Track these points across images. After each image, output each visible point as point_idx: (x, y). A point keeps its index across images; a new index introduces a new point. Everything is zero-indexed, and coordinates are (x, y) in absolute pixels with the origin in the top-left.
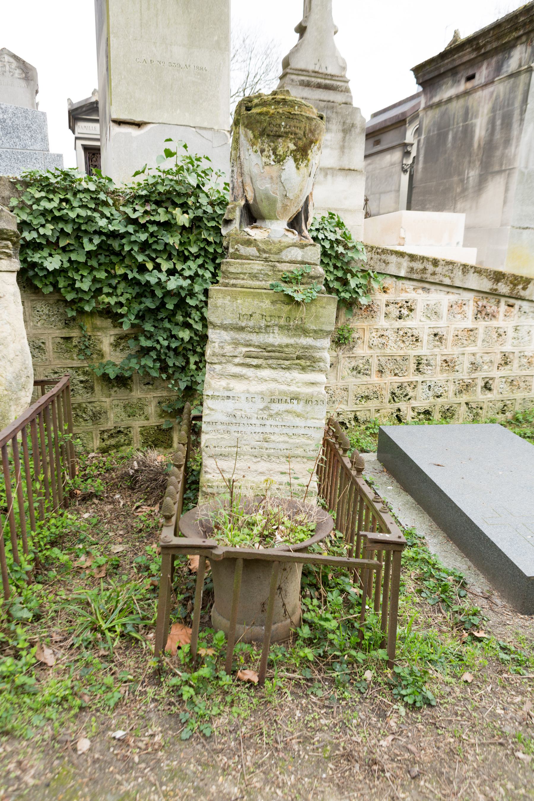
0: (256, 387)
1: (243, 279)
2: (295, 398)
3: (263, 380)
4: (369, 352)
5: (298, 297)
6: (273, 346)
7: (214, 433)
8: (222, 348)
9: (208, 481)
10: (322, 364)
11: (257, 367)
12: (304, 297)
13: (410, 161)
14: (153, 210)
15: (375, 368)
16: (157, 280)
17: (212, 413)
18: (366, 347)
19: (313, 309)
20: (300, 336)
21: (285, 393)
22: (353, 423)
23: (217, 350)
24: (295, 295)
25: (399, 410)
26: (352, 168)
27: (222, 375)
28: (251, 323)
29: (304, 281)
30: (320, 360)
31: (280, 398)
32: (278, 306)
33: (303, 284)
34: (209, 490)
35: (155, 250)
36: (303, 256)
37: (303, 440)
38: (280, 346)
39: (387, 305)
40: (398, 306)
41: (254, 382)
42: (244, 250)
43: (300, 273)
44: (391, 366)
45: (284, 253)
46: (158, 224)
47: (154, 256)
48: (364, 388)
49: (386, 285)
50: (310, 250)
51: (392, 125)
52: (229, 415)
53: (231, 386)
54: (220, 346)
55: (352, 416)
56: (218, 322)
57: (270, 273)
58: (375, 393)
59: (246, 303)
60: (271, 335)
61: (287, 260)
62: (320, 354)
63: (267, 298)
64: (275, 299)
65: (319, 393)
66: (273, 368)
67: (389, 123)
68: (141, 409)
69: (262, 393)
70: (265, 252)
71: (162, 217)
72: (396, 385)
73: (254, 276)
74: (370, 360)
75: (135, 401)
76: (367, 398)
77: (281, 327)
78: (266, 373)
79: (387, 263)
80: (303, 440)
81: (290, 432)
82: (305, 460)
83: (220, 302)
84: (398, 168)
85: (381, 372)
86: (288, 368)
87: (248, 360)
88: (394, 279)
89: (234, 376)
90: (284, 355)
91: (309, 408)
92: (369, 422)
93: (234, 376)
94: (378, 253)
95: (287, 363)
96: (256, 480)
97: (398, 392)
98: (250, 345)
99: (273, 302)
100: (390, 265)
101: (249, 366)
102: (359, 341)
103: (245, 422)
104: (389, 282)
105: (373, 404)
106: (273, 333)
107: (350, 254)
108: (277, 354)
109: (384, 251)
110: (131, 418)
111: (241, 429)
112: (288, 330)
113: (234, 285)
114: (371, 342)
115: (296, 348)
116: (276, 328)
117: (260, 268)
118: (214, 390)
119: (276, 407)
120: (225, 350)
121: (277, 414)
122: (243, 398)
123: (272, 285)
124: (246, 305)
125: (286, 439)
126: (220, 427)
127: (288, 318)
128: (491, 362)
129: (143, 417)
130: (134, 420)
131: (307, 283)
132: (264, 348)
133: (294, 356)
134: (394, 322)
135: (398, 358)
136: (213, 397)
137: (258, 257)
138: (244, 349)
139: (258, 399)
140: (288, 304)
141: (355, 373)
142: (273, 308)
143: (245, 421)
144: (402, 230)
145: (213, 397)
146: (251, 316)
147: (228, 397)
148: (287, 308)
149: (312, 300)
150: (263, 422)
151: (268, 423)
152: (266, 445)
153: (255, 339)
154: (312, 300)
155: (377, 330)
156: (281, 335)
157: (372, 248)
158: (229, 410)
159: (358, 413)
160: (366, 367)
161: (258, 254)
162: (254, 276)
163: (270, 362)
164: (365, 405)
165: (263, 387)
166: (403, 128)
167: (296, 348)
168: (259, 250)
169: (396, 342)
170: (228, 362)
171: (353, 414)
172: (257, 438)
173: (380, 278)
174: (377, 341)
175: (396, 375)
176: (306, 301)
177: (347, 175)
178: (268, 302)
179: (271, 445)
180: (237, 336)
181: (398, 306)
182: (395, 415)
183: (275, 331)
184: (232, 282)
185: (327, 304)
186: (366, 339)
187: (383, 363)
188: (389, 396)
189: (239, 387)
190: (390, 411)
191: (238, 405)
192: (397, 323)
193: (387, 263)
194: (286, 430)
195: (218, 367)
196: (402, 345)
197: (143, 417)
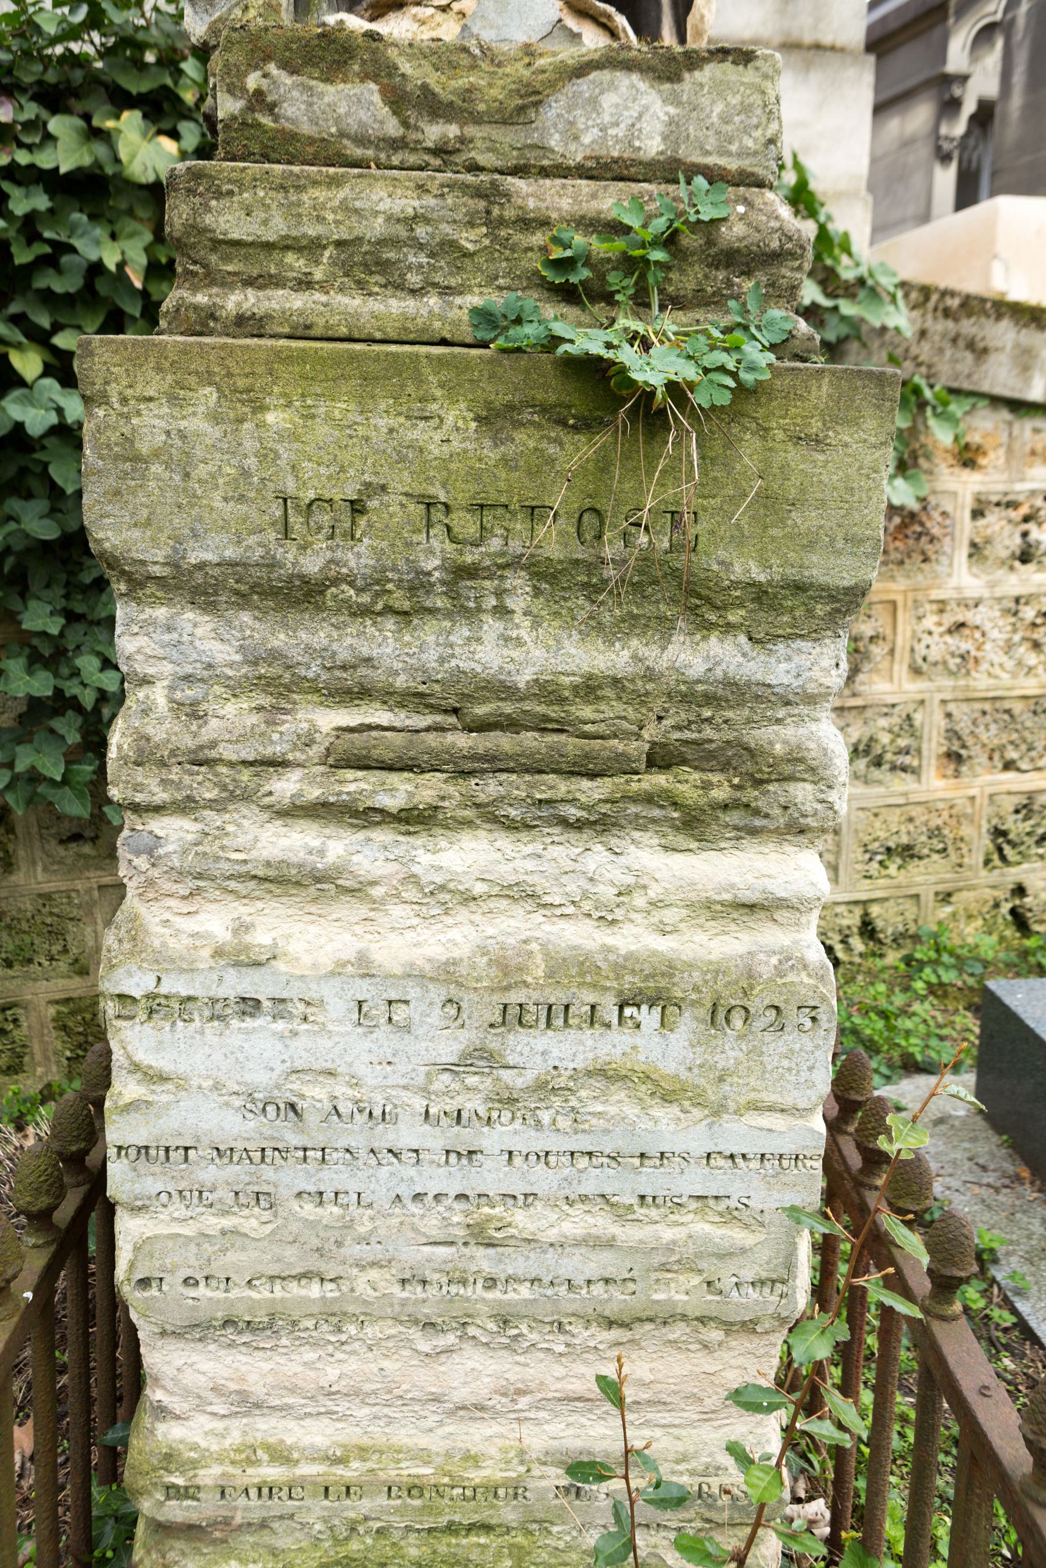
0: (408, 941)
1: (305, 284)
2: (650, 992)
3: (448, 897)
4: (913, 688)
5: (652, 370)
6: (505, 691)
7: (177, 1209)
8: (194, 712)
9: (169, 1459)
10: (803, 793)
11: (414, 819)
12: (689, 372)
13: (960, 128)
14: (30, 126)
15: (934, 744)
16: (53, 419)
17: (162, 1095)
18: (901, 669)
19: (749, 452)
20: (665, 628)
21: (582, 968)
22: (858, 944)
23: (164, 729)
24: (628, 355)
25: (1020, 891)
26: (827, 39)
27: (201, 879)
28: (359, 558)
29: (686, 281)
30: (798, 766)
31: (557, 997)
32: (525, 440)
33: (674, 302)
34: (176, 1511)
35: (47, 297)
36: (673, 131)
37: (705, 1228)
38: (546, 690)
39: (977, 514)
40: (1017, 515)
41: (398, 911)
42: (315, 105)
43: (659, 224)
44: (991, 735)
45: (554, 110)
46: (51, 181)
47: (44, 321)
48: (894, 817)
49: (975, 438)
50: (720, 88)
51: (905, 27)
52: (259, 1105)
53: (261, 938)
54: (177, 706)
55: (853, 920)
56: (152, 554)
57: (469, 239)
58: (935, 833)
59: (322, 431)
60: (492, 627)
61: (576, 155)
62: (789, 732)
63: (452, 391)
64: (501, 399)
65: (790, 962)
66: (511, 826)
67: (894, 25)
68: (56, 933)
69: (447, 973)
70: (434, 106)
71: (66, 153)
72: (1009, 804)
73: (368, 263)
74: (918, 718)
75: (28, 906)
76: (907, 852)
77: (545, 575)
78: (468, 855)
79: (980, 351)
80: (702, 1227)
81: (624, 1186)
82: (715, 1335)
83: (152, 425)
84: (924, 151)
85: (955, 758)
86: (599, 824)
87: (356, 784)
88: (1005, 414)
89: (280, 880)
90: (570, 744)
91: (729, 1050)
92: (916, 938)
93: (280, 880)
94: (947, 313)
95: (592, 790)
96: (435, 1443)
97: (1016, 826)
98: (362, 694)
99: (492, 419)
100: (993, 358)
101: (363, 816)
102: (878, 651)
103: (358, 1141)
104: (985, 426)
105: (925, 876)
106: (502, 611)
107: (847, 308)
108: (530, 739)
109: (973, 306)
110: (17, 970)
111: (331, 1178)
112: (592, 590)
113: (248, 324)
114: (921, 650)
115: (641, 699)
116: (518, 581)
117: (407, 203)
118: (163, 962)
119: (536, 1051)
120: (212, 729)
121: (543, 1088)
122: (338, 1007)
123: (484, 316)
124: (318, 437)
125: (602, 1223)
126: (209, 1173)
127: (591, 518)
128: (916, 671)
129: (63, 966)
130: (28, 977)
131: (702, 300)
132: (454, 702)
133: (637, 748)
134: (1001, 573)
135: (1018, 707)
136: (155, 1006)
137: (397, 144)
138: (330, 719)
139: (425, 1009)
140: (586, 425)
141: (862, 764)
142: (492, 455)
143: (356, 1134)
144: (997, 268)
145: (155, 1006)
146: (357, 508)
147: (249, 1006)
148: (576, 452)
149: (742, 391)
150: (464, 1137)
151: (493, 1140)
152: (483, 1260)
153: (391, 649)
154: (742, 391)
155: (942, 606)
156: (551, 627)
157: (926, 291)
158: (260, 1078)
159: (875, 910)
160: (902, 742)
161: (392, 128)
162: (368, 263)
163: (490, 788)
164: (902, 877)
165: (456, 938)
166: (937, 33)
167: (641, 699)
168: (397, 99)
169: (1009, 647)
170: (234, 797)
171: (858, 911)
172: (432, 1225)
173: (956, 408)
174: (939, 647)
175: (1009, 766)
176: (700, 399)
177: (808, 66)
178: (456, 415)
179: (518, 1263)
180: (280, 640)
181: (1017, 515)
182: (1006, 908)
183: (516, 603)
184: (237, 301)
185: (834, 419)
186: (902, 639)
187: (964, 726)
188: (986, 842)
189: (305, 940)
190: (989, 894)
191: (305, 1049)
192: (1013, 578)
193: (980, 351)
194: (594, 1180)
195: (174, 831)
196: (1032, 659)
197: (63, 966)
